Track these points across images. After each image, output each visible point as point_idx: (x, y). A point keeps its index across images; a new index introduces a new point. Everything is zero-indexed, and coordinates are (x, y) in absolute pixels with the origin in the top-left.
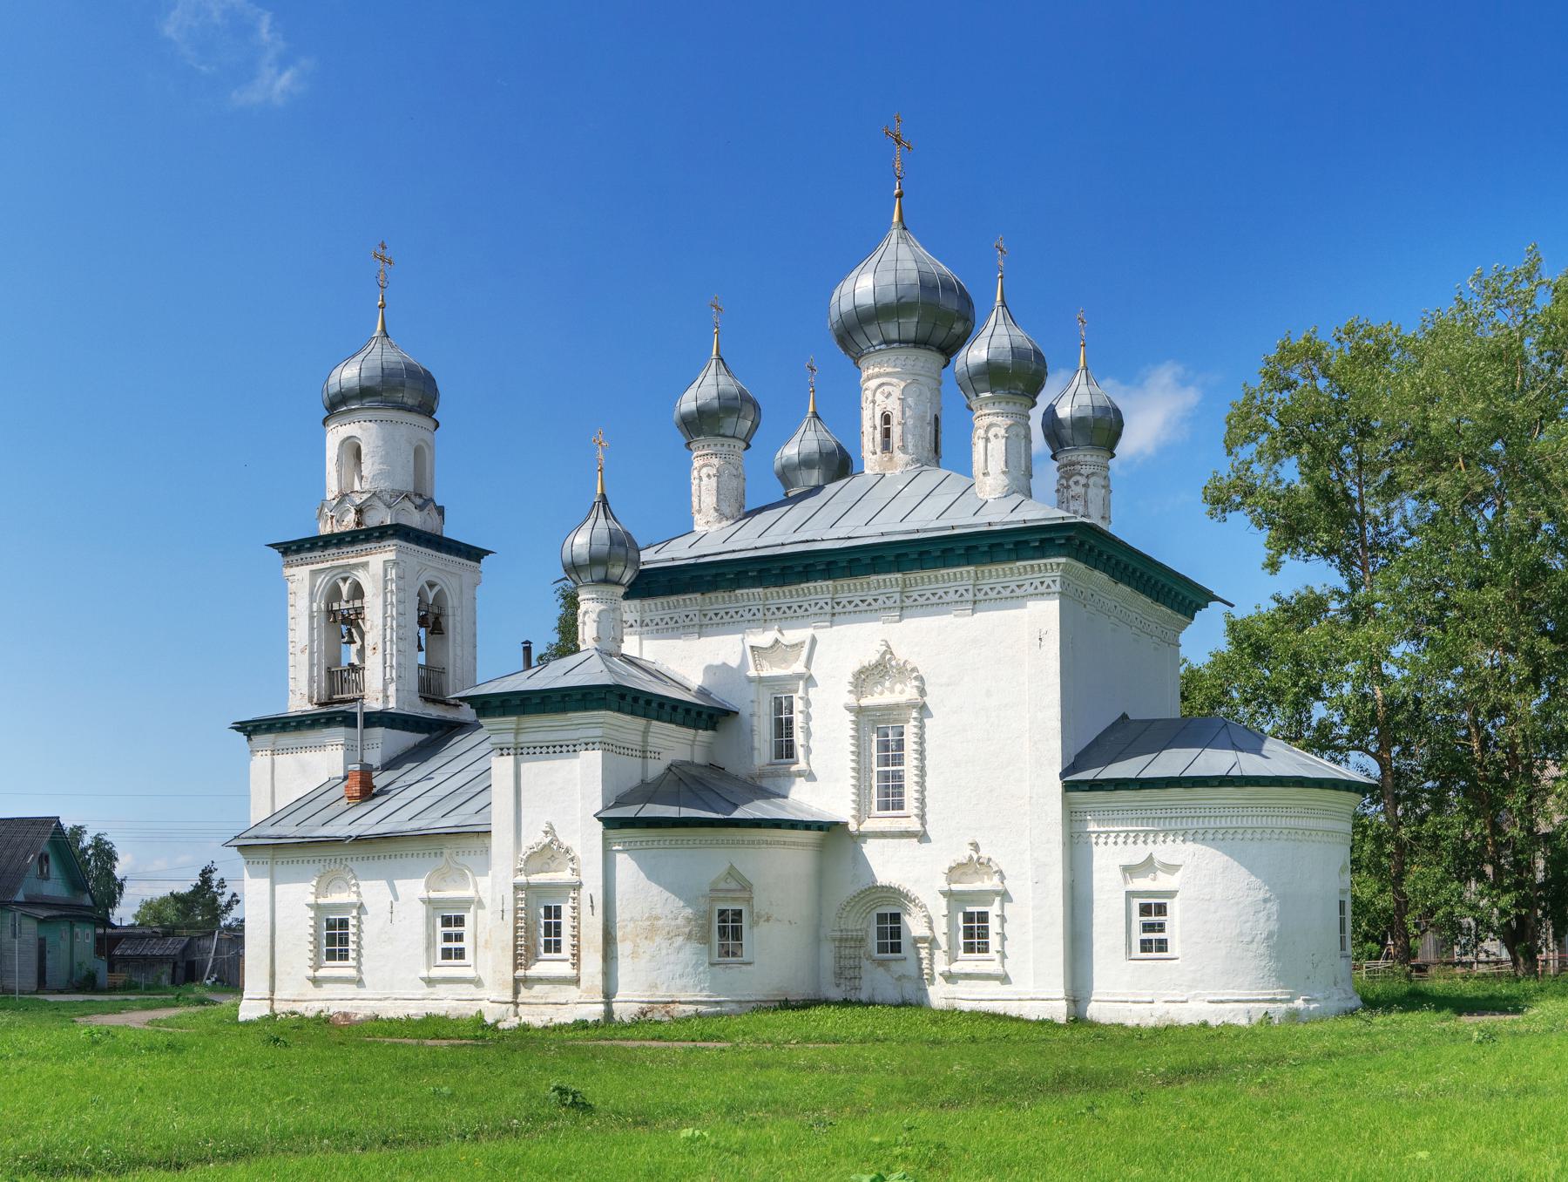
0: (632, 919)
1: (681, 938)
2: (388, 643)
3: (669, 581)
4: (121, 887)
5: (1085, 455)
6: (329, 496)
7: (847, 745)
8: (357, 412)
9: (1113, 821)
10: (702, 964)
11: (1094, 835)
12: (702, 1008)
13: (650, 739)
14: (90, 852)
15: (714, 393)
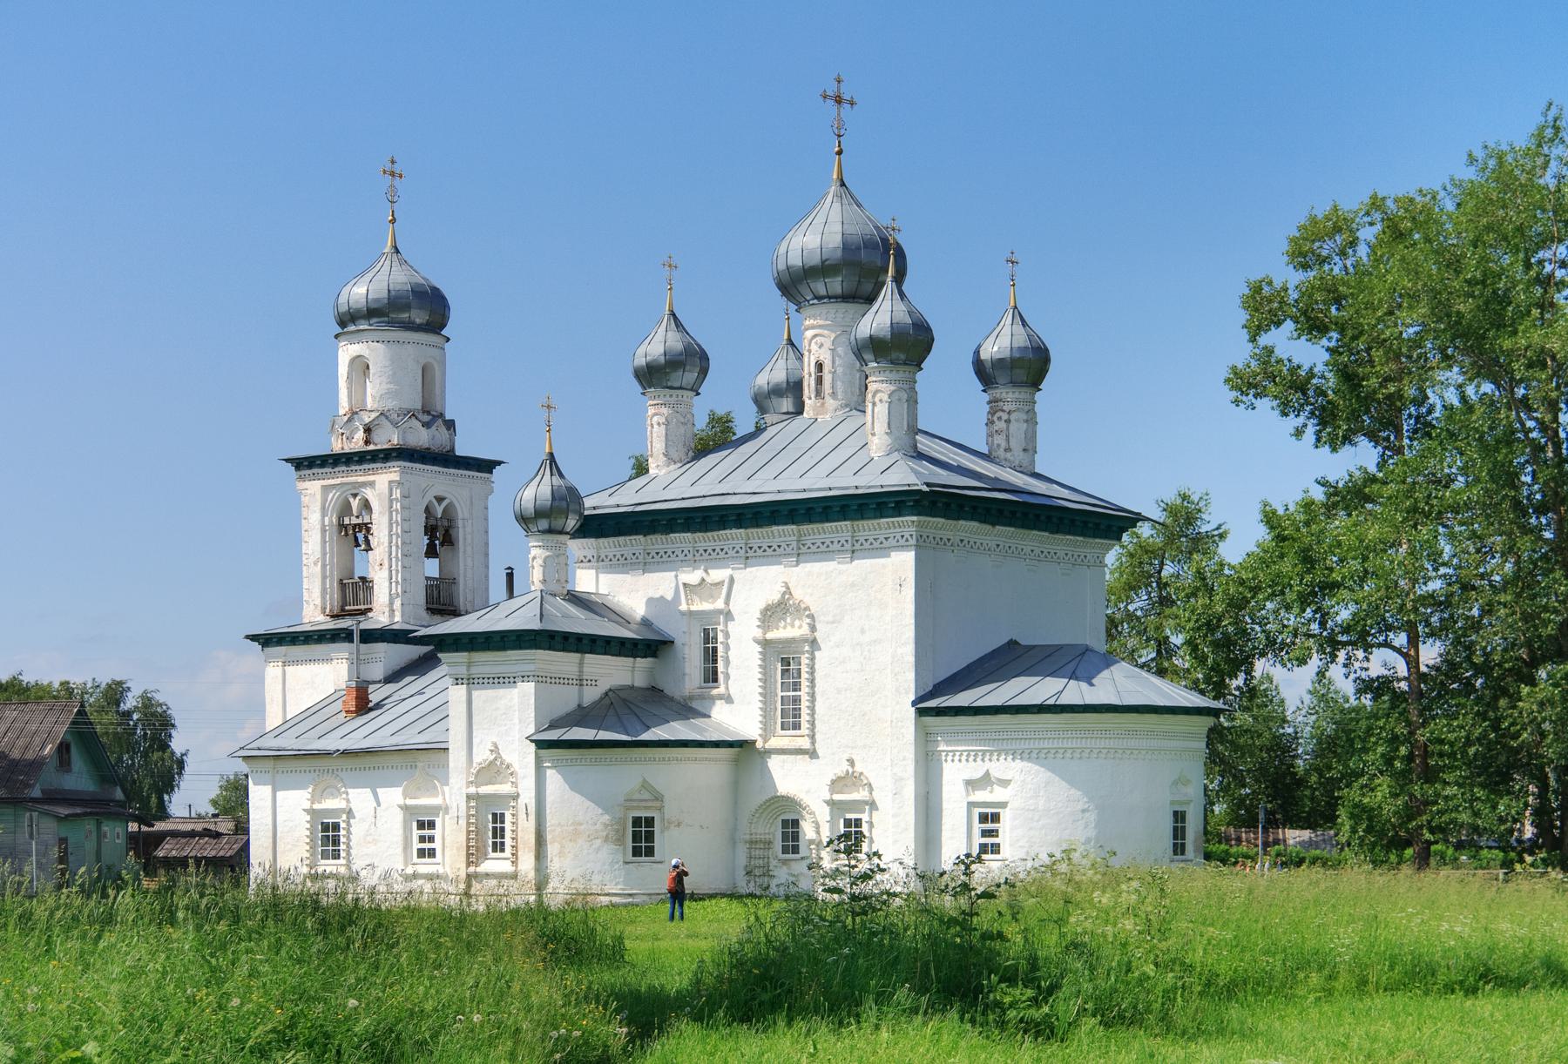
0: (559, 824)
1: (599, 841)
2: (394, 560)
3: (617, 524)
4: (181, 764)
5: (1007, 393)
6: (342, 412)
7: (756, 673)
8: (366, 333)
9: (959, 742)
10: (617, 863)
11: (944, 754)
12: (615, 900)
13: (585, 669)
14: (135, 717)
15: (662, 351)
